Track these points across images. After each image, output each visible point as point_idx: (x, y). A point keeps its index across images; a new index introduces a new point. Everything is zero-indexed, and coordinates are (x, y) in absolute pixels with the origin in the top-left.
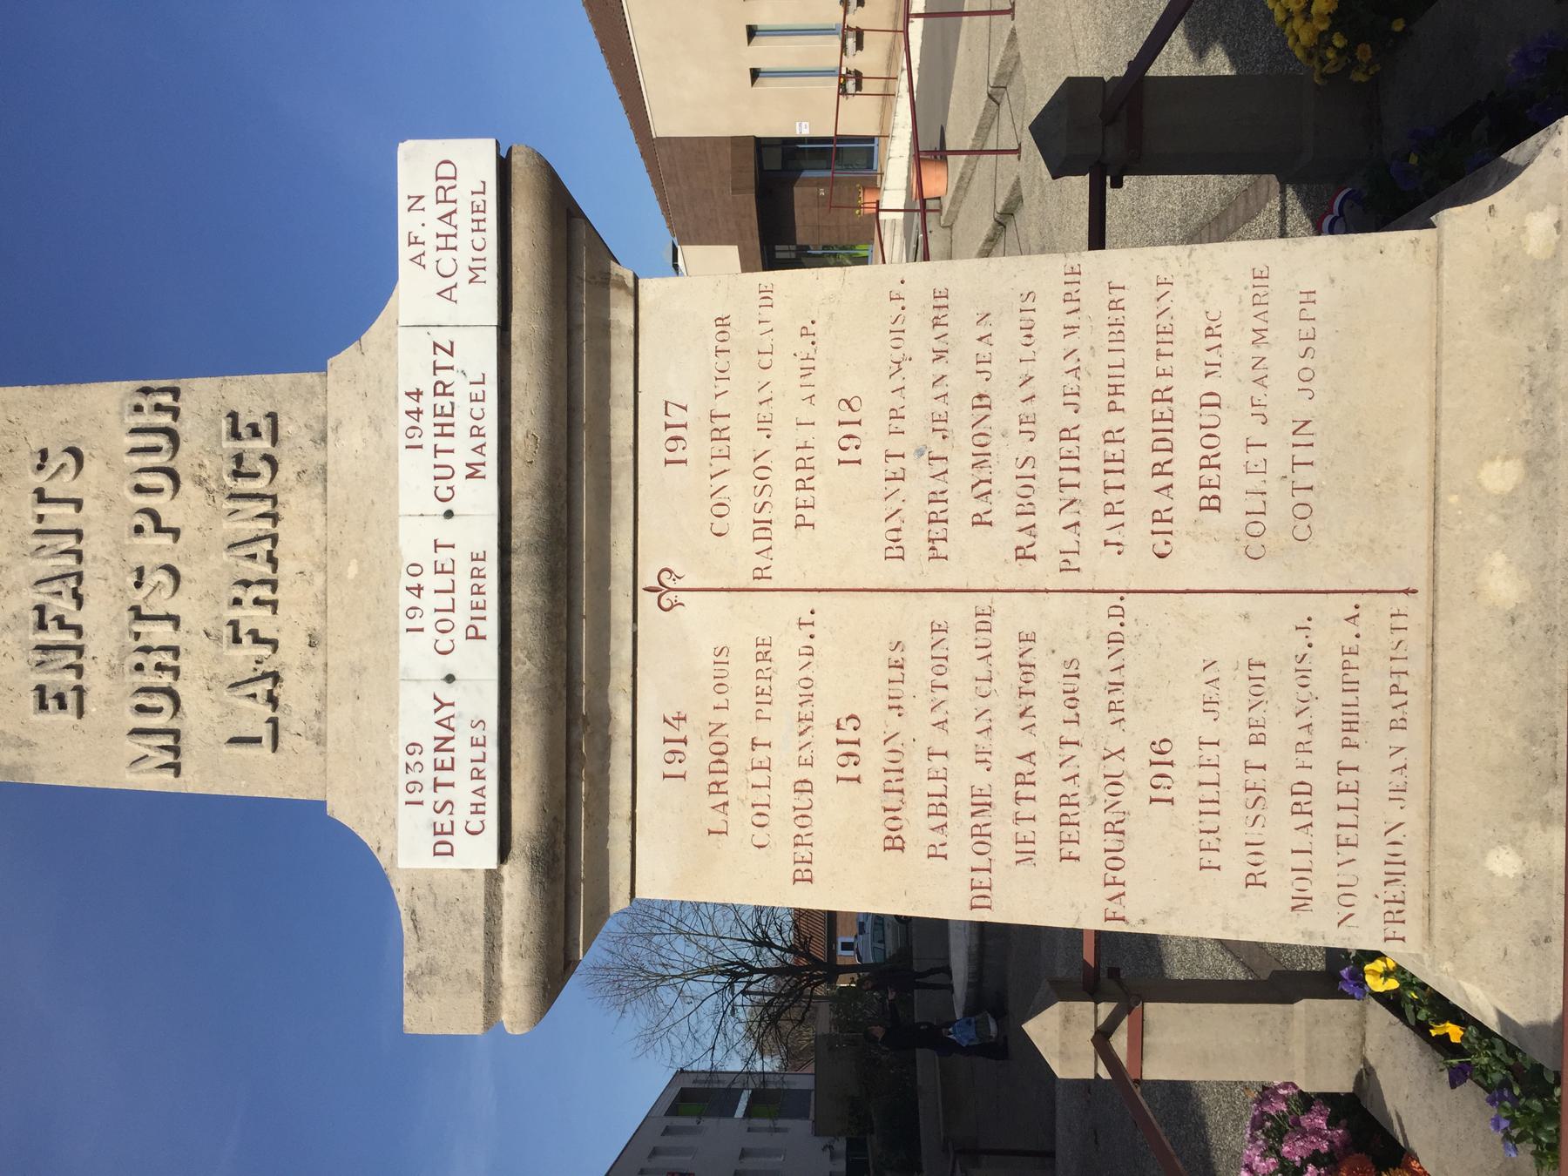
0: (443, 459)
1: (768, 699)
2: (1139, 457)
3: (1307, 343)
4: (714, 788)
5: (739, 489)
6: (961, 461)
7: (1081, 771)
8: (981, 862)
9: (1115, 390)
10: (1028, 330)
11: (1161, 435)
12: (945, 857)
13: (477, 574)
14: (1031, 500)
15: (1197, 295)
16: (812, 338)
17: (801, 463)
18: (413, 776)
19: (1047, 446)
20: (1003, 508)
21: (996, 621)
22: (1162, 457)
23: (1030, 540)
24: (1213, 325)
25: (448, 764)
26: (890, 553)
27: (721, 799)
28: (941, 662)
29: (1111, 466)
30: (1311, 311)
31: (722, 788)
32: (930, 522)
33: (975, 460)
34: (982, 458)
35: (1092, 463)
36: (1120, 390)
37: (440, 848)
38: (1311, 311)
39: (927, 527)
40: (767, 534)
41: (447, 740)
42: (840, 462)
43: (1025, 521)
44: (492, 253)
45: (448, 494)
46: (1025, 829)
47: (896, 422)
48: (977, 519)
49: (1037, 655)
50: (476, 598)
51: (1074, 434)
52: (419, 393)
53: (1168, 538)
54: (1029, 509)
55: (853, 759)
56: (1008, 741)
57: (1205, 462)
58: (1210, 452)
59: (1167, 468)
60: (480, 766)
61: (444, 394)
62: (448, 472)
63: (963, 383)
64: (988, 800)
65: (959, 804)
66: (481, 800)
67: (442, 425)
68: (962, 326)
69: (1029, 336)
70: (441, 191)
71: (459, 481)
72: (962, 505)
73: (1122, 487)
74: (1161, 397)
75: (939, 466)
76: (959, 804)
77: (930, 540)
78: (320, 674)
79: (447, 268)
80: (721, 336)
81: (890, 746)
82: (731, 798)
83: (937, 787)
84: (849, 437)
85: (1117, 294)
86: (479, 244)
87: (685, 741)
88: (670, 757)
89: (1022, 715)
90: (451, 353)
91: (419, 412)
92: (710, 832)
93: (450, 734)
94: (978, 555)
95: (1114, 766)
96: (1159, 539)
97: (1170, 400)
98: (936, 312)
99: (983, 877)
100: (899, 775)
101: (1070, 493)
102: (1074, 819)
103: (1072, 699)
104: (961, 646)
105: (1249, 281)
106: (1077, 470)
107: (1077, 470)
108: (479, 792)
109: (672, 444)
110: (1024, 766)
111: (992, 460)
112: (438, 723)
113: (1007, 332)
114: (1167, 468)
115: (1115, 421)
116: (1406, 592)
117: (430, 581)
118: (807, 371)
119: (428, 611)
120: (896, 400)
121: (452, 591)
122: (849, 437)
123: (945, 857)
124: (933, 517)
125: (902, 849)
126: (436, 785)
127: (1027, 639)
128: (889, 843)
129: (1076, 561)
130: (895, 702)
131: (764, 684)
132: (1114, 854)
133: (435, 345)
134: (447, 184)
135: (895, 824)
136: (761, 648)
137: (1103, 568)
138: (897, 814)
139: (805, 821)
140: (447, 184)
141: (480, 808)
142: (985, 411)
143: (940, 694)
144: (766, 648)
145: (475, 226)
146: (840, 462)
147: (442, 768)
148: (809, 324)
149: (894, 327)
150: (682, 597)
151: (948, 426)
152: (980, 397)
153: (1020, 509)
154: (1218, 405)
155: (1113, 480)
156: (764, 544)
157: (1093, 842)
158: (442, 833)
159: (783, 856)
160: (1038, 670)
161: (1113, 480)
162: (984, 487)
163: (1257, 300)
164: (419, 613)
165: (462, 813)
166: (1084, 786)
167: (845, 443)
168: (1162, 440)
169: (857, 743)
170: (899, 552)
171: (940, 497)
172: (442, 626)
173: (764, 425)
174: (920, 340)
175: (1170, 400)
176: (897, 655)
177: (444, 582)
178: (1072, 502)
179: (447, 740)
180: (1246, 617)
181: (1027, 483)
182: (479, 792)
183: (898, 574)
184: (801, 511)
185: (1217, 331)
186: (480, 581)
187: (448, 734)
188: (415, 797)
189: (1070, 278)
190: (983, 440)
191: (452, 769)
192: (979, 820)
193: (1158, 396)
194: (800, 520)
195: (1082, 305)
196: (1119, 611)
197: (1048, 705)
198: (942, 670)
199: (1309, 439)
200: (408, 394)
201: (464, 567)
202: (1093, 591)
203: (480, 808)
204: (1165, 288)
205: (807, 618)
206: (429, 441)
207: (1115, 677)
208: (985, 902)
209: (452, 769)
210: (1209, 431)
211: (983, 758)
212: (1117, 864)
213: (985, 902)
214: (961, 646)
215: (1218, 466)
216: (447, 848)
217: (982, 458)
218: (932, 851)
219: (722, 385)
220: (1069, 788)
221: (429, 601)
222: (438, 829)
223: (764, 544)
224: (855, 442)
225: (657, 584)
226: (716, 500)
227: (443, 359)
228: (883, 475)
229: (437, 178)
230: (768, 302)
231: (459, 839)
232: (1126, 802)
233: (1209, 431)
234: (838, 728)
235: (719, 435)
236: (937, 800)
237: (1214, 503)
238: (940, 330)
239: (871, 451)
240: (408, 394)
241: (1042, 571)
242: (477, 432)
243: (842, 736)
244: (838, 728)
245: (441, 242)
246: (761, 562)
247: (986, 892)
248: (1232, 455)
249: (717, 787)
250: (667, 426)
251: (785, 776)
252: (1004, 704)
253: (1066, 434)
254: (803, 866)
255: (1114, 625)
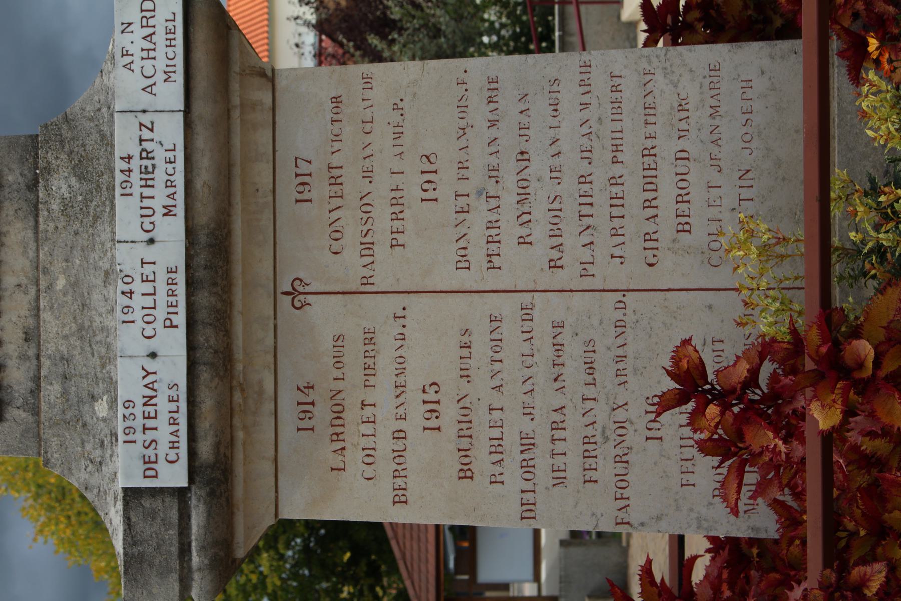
0: (146, 203)
1: (372, 372)
2: (634, 196)
3: (747, 116)
4: (335, 437)
5: (350, 220)
6: (509, 199)
7: (598, 419)
8: (528, 486)
9: (616, 149)
10: (555, 106)
11: (649, 180)
12: (502, 483)
13: (171, 283)
14: (559, 226)
15: (672, 82)
16: (401, 112)
17: (394, 201)
18: (129, 423)
19: (569, 186)
20: (539, 232)
21: (536, 313)
22: (650, 195)
23: (558, 255)
24: (683, 103)
25: (152, 414)
26: (460, 265)
27: (339, 445)
28: (497, 343)
29: (614, 202)
30: (749, 94)
31: (341, 437)
32: (488, 242)
33: (519, 198)
34: (523, 197)
35: (601, 200)
36: (620, 148)
37: (149, 473)
38: (749, 94)
39: (485, 246)
40: (371, 252)
41: (152, 397)
42: (423, 200)
43: (555, 241)
44: (179, 61)
45: (150, 227)
46: (559, 461)
47: (462, 171)
48: (521, 240)
49: (565, 337)
50: (170, 299)
51: (588, 179)
52: (130, 158)
53: (655, 252)
54: (557, 233)
55: (435, 414)
56: (545, 399)
57: (680, 199)
58: (683, 192)
59: (654, 203)
60: (175, 415)
61: (147, 158)
62: (150, 212)
63: (508, 140)
64: (532, 441)
65: (512, 442)
66: (176, 439)
67: (146, 180)
68: (508, 103)
69: (556, 110)
70: (144, 20)
71: (158, 218)
72: (510, 231)
73: (623, 217)
74: (649, 153)
75: (493, 203)
76: (512, 442)
77: (488, 256)
78: (34, 362)
79: (149, 71)
80: (335, 110)
81: (461, 404)
82: (347, 444)
83: (496, 433)
84: (429, 182)
85: (617, 81)
86: (171, 55)
87: (313, 403)
88: (302, 415)
89: (555, 380)
90: (152, 130)
91: (130, 171)
92: (332, 469)
93: (153, 393)
94: (521, 266)
95: (620, 415)
96: (649, 253)
97: (655, 155)
98: (489, 93)
99: (529, 497)
100: (468, 425)
101: (587, 221)
102: (593, 454)
103: (590, 368)
104: (510, 331)
105: (706, 72)
106: (591, 204)
107: (591, 204)
108: (174, 433)
109: (301, 188)
110: (557, 417)
111: (531, 198)
112: (145, 386)
113: (540, 106)
114: (654, 203)
115: (617, 170)
116: (132, 242)
117: (139, 287)
118: (398, 135)
119: (137, 308)
120: (462, 156)
121: (154, 294)
122: (429, 182)
123: (502, 483)
124: (490, 239)
125: (471, 478)
126: (145, 429)
127: (558, 325)
128: (462, 474)
129: (591, 270)
130: (465, 373)
131: (370, 361)
132: (621, 477)
133: (141, 124)
134: (148, 14)
135: (466, 460)
136: (367, 335)
137: (609, 273)
138: (467, 453)
139: (401, 460)
140: (148, 14)
141: (176, 445)
142: (525, 163)
143: (497, 366)
144: (371, 335)
145: (168, 43)
146: (423, 200)
147: (149, 417)
148: (399, 102)
149: (460, 104)
150: (310, 298)
151: (501, 174)
152: (522, 153)
153: (551, 233)
154: (688, 159)
155: (616, 212)
156: (369, 260)
157: (606, 470)
158: (150, 462)
159: (386, 487)
160: (566, 348)
161: (616, 212)
162: (526, 218)
163: (712, 85)
164: (131, 310)
165: (163, 448)
166: (600, 430)
167: (426, 186)
168: (650, 184)
169: (438, 402)
170: (466, 265)
171: (495, 225)
172: (147, 319)
173: (368, 174)
174: (478, 113)
175: (655, 155)
176: (465, 339)
177: (148, 288)
178: (588, 228)
179: (152, 397)
180: (710, 307)
181: (556, 214)
182: (174, 433)
183: (466, 280)
184: (395, 236)
185: (686, 107)
186: (173, 287)
187: (152, 393)
188: (131, 437)
189: (583, 69)
190: (524, 184)
191: (155, 417)
192: (526, 456)
193: (646, 152)
194: (394, 242)
195: (592, 88)
196: (622, 305)
197: (573, 371)
198: (497, 349)
199: (750, 183)
200: (122, 158)
201: (162, 277)
202: (604, 291)
203: (176, 445)
204: (649, 77)
205: (400, 313)
206: (136, 190)
207: (620, 352)
208: (532, 514)
209: (155, 417)
210: (682, 177)
211: (528, 411)
212: (624, 484)
213: (532, 514)
214: (510, 331)
215: (689, 202)
216: (152, 473)
217: (523, 197)
218: (493, 479)
219: (337, 145)
220: (590, 431)
221: (138, 301)
222: (147, 460)
223: (369, 260)
224: (434, 186)
225: (290, 290)
226: (333, 228)
227: (146, 134)
228: (454, 209)
229: (142, 11)
230: (369, 85)
231: (162, 467)
232: (630, 439)
233: (682, 177)
234: (424, 391)
235: (335, 182)
236: (496, 442)
237: (687, 227)
238: (492, 106)
239: (445, 192)
240: (122, 158)
241: (566, 278)
242: (169, 184)
243: (427, 397)
244: (424, 391)
245: (145, 54)
246: (367, 272)
247: (532, 507)
248: (697, 194)
249: (337, 437)
250: (297, 175)
251: (387, 426)
252: (542, 374)
253: (583, 180)
254: (400, 493)
255: (619, 314)
